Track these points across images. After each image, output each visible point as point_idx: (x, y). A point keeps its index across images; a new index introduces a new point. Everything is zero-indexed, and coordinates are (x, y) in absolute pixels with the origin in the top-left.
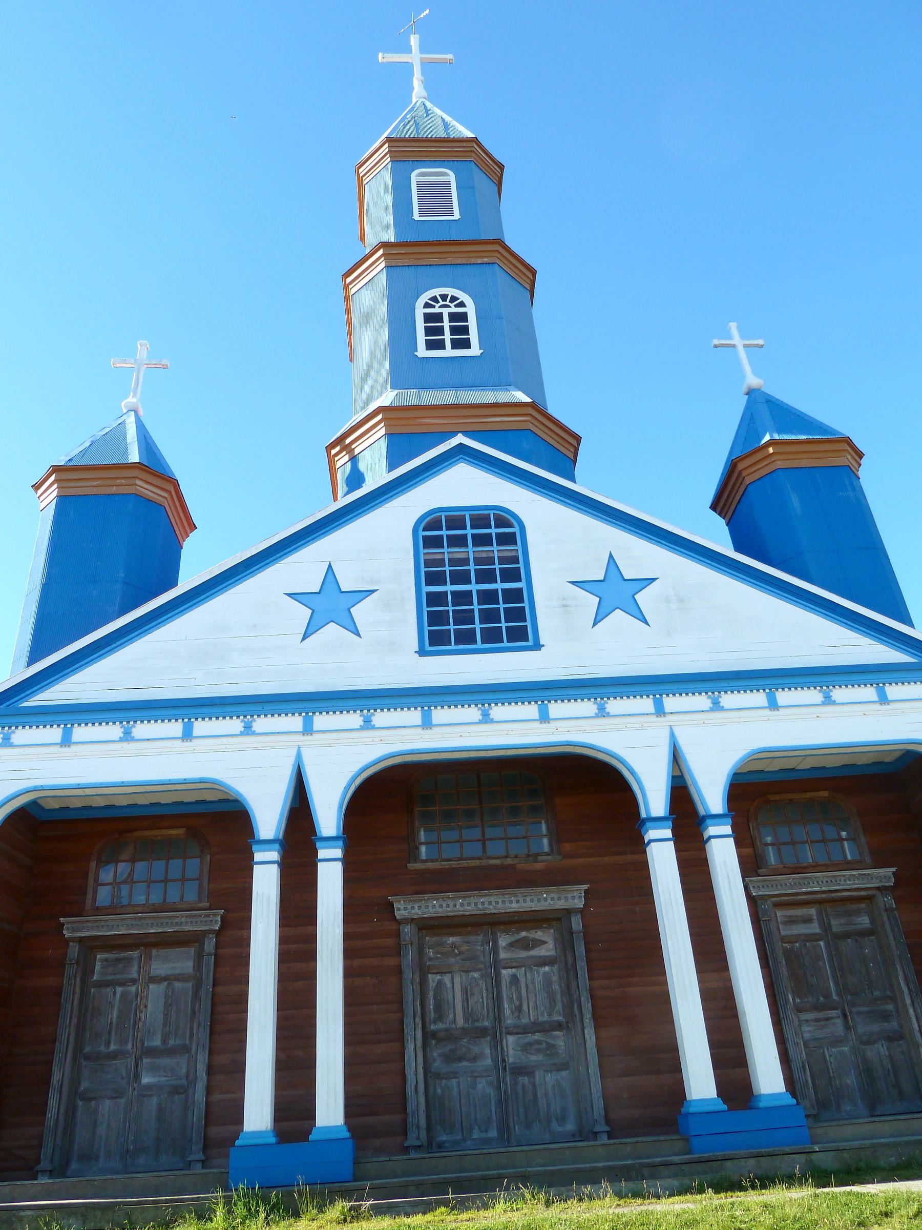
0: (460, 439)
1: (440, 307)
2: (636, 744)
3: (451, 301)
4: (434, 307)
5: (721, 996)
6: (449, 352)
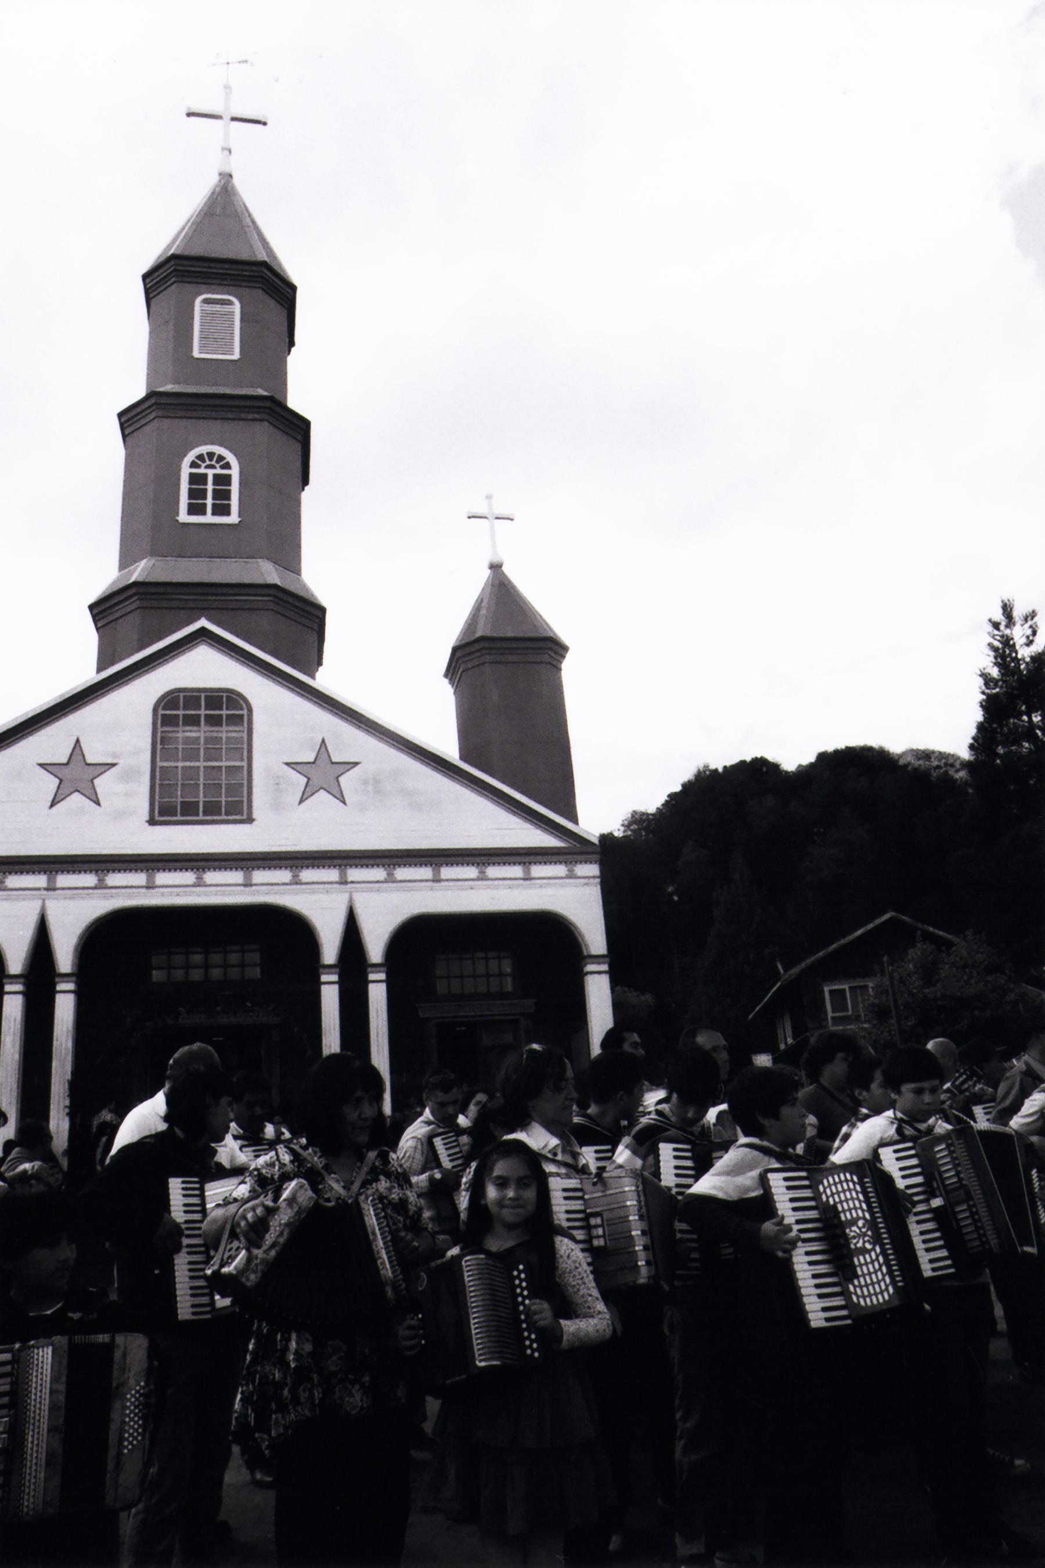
0: (203, 623)
1: (207, 467)
3: (217, 462)
4: (199, 466)
6: (209, 518)
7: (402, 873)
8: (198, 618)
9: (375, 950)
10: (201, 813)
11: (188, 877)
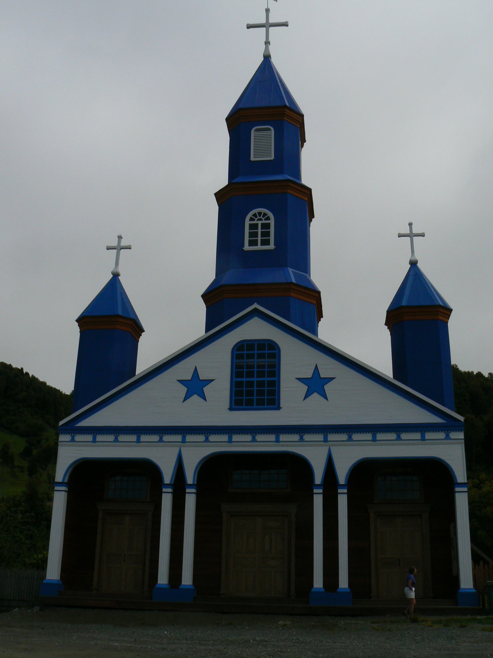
0: (255, 306)
1: (258, 220)
2: (315, 456)
3: (263, 217)
4: (254, 220)
5: (331, 550)
6: (259, 247)
7: (356, 436)
8: (253, 304)
9: (342, 476)
10: (255, 405)
11: (248, 438)
